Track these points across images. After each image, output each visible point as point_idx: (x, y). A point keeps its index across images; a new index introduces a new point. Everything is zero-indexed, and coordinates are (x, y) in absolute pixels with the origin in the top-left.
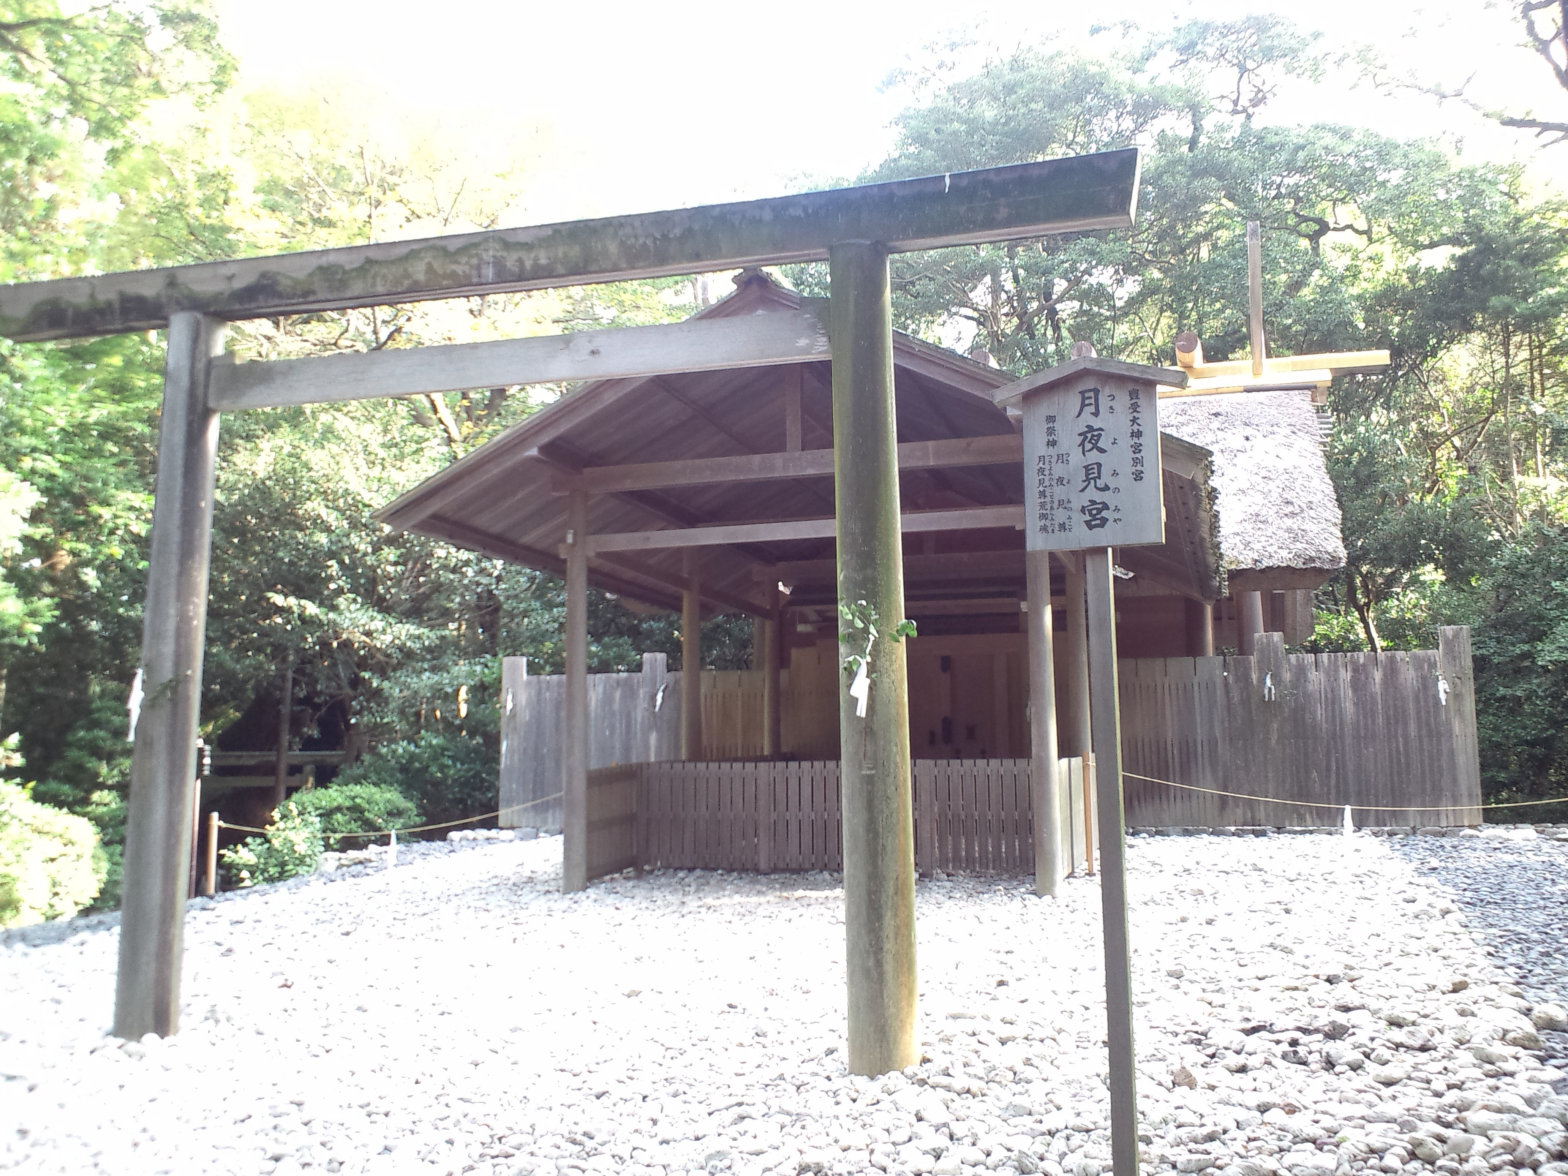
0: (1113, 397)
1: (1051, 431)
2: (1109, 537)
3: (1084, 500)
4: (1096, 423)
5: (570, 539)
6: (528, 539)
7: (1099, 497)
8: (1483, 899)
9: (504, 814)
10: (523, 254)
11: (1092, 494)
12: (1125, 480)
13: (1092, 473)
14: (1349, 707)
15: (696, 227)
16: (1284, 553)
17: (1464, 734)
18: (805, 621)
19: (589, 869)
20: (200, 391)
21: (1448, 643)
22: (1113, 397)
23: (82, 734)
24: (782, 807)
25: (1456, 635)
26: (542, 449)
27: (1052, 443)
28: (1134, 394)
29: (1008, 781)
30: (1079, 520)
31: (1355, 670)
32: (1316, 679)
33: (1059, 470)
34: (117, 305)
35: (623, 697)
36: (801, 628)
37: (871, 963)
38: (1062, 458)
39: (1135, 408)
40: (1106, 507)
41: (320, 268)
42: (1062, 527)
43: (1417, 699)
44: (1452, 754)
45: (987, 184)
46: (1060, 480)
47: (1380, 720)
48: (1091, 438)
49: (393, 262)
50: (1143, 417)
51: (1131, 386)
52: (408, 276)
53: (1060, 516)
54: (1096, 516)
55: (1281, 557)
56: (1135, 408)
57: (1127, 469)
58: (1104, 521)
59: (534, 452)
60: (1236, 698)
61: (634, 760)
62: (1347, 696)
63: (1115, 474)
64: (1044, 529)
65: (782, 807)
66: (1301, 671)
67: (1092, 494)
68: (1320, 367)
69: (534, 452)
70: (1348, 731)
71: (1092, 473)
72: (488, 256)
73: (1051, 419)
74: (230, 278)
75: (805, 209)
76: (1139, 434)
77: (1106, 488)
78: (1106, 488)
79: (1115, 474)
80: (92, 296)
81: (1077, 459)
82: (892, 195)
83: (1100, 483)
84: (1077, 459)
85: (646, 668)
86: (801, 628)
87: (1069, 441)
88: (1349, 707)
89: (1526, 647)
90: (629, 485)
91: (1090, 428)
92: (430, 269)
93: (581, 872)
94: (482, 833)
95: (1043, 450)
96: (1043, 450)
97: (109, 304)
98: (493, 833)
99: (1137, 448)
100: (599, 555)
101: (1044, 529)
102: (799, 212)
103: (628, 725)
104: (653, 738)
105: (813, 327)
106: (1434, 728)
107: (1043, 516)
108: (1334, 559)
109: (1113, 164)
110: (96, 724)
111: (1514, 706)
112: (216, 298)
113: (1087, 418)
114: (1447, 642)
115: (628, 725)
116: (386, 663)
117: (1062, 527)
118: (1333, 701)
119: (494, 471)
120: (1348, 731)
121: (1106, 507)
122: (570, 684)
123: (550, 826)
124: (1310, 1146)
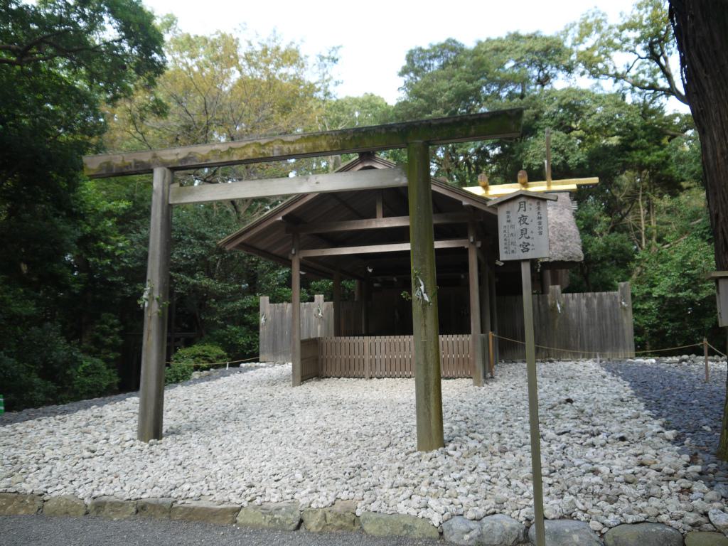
0: (531, 205)
1: (508, 217)
2: (529, 255)
3: (521, 241)
4: (525, 214)
5: (293, 252)
6: (275, 252)
7: (526, 241)
8: (643, 387)
9: (261, 357)
10: (289, 146)
11: (524, 240)
12: (535, 235)
13: (523, 232)
14: (585, 314)
15: (356, 136)
16: (560, 255)
17: (628, 321)
18: (377, 282)
19: (302, 377)
20: (166, 198)
21: (622, 289)
22: (531, 205)
23: (98, 326)
24: (374, 353)
25: (625, 286)
26: (283, 217)
27: (509, 221)
28: (538, 203)
29: (460, 343)
30: (519, 249)
31: (587, 299)
32: (572, 303)
33: (511, 231)
34: (133, 165)
35: (307, 312)
36: (375, 285)
37: (426, 410)
38: (513, 227)
39: (539, 208)
40: (529, 244)
41: (212, 151)
42: (513, 252)
43: (610, 311)
44: (623, 331)
45: (466, 120)
46: (512, 234)
47: (596, 319)
48: (523, 219)
49: (240, 149)
50: (542, 211)
51: (537, 201)
52: (245, 154)
53: (512, 248)
54: (525, 249)
55: (559, 256)
56: (539, 208)
57: (536, 231)
58: (528, 250)
59: (280, 218)
60: (542, 310)
61: (312, 337)
62: (584, 309)
63: (532, 232)
64: (506, 252)
65: (374, 353)
66: (567, 299)
67: (524, 240)
68: (571, 184)
69: (280, 218)
70: (584, 323)
71: (523, 232)
72: (276, 147)
73: (508, 212)
74: (177, 154)
75: (398, 128)
76: (541, 218)
77: (529, 238)
78: (529, 238)
79: (532, 232)
80: (123, 161)
81: (518, 227)
82: (430, 124)
83: (527, 236)
84: (518, 227)
85: (316, 300)
86: (375, 285)
87: (515, 220)
88: (585, 314)
89: (649, 289)
90: (316, 231)
91: (523, 216)
92: (254, 151)
93: (299, 379)
94: (253, 364)
95: (505, 224)
96: (505, 224)
97: (130, 164)
98: (258, 364)
99: (540, 223)
100: (304, 258)
101: (506, 252)
102: (395, 130)
103: (309, 325)
104: (319, 327)
105: (401, 174)
106: (617, 324)
107: (506, 248)
108: (579, 257)
109: (514, 113)
110: (103, 323)
111: (646, 312)
112: (172, 162)
113: (522, 212)
114: (622, 289)
115: (309, 325)
116: (220, 298)
117: (513, 252)
118: (579, 312)
119: (265, 225)
120: (584, 323)
121: (529, 244)
122: (293, 308)
123: (279, 361)
124: (591, 474)
